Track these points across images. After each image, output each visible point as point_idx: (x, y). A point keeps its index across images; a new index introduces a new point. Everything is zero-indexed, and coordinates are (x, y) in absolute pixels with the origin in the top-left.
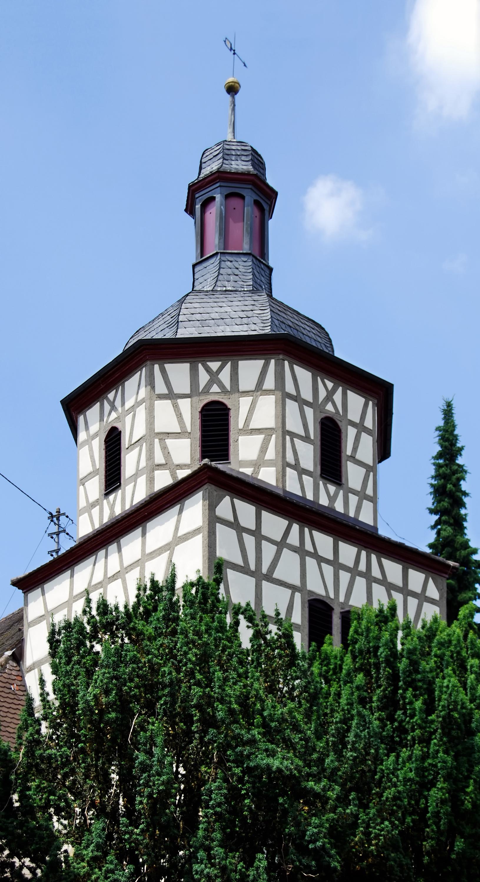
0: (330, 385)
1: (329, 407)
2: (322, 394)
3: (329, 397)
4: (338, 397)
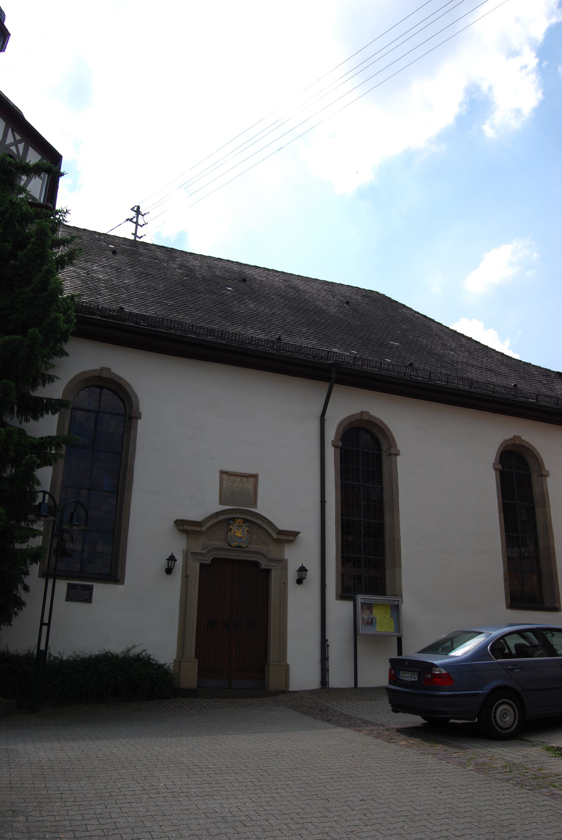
0: (18, 137)
1: (13, 148)
2: (10, 139)
3: (16, 143)
4: (21, 146)
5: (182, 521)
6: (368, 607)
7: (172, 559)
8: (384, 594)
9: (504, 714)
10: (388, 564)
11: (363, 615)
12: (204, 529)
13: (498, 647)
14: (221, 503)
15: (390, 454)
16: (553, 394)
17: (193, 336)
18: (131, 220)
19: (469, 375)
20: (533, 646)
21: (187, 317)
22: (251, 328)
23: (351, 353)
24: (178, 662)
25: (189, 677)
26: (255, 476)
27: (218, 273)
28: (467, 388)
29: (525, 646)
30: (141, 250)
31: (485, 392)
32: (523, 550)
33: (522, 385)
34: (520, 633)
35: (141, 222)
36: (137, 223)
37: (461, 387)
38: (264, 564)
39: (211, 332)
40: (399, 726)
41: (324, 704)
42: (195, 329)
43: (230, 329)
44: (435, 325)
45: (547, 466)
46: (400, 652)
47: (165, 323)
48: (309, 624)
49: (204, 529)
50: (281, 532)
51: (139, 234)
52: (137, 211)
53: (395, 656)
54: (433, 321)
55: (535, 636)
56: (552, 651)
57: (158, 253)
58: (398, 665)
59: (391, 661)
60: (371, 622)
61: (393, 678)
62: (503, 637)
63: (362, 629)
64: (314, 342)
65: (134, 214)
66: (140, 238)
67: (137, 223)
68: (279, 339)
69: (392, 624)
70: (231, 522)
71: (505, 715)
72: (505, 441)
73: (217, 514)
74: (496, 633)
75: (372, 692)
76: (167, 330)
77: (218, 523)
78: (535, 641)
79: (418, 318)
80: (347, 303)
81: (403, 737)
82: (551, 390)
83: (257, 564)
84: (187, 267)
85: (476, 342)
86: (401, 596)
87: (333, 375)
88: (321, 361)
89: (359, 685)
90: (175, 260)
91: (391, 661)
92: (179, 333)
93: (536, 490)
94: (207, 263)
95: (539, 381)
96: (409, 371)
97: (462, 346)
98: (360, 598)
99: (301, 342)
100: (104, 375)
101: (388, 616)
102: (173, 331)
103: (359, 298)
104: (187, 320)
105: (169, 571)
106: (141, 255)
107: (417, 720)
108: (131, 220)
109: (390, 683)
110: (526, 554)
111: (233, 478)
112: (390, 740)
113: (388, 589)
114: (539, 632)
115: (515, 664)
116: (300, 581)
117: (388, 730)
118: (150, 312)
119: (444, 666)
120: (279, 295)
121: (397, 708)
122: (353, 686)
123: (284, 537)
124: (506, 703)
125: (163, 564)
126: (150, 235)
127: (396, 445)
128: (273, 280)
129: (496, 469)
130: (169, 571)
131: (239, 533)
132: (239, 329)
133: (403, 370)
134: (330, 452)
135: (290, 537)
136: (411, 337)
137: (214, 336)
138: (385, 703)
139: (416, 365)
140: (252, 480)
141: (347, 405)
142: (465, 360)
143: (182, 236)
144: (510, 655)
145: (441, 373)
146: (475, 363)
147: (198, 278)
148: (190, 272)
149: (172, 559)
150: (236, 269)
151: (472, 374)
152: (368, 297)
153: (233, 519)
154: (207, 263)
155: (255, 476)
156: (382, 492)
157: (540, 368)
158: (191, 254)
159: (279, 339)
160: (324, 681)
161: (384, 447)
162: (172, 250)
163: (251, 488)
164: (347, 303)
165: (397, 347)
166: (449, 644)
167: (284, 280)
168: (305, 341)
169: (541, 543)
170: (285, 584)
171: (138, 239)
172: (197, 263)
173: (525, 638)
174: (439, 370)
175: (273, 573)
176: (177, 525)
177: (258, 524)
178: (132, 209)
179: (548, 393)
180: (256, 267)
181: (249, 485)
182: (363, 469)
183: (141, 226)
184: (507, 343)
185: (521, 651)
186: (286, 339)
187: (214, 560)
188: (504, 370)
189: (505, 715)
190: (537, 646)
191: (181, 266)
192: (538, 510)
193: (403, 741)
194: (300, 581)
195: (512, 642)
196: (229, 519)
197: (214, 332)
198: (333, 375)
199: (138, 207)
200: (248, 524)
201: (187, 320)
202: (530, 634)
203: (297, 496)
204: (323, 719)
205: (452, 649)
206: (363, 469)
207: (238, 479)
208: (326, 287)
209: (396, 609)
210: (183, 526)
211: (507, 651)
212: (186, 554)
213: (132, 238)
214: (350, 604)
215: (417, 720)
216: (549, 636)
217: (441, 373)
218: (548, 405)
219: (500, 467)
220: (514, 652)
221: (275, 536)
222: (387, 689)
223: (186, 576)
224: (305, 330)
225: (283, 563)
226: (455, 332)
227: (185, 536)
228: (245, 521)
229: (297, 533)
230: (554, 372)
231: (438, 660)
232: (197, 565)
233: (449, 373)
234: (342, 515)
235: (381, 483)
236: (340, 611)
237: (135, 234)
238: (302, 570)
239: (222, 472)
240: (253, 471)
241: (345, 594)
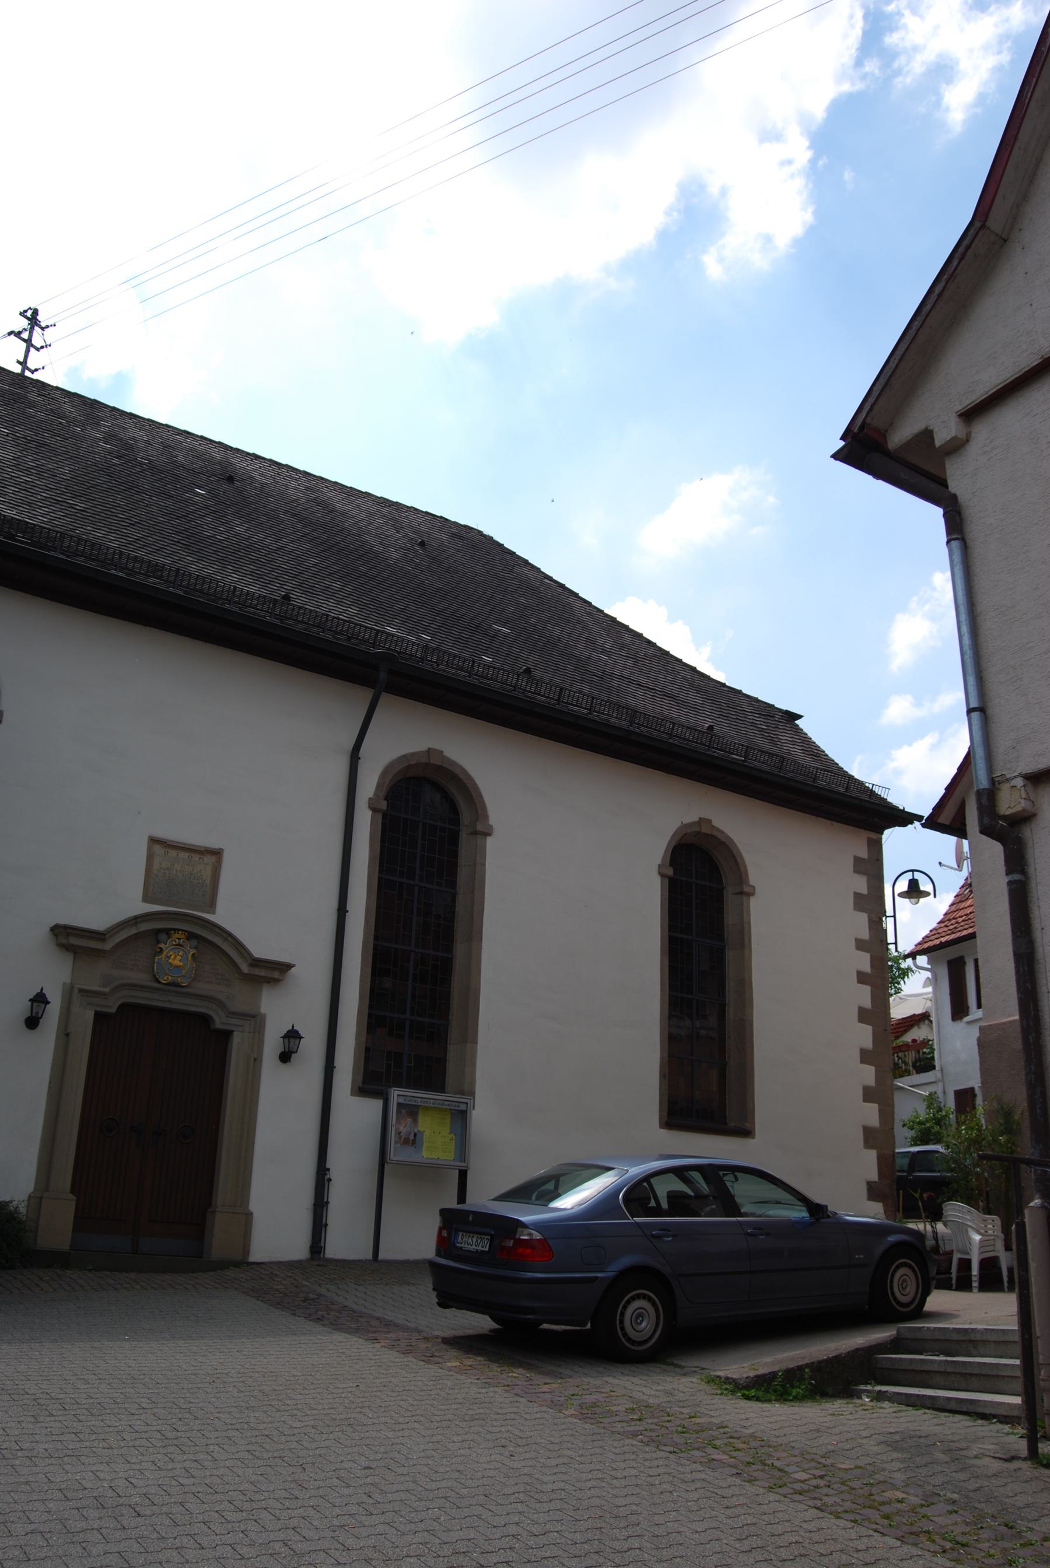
5: (66, 927)
6: (411, 1111)
7: (40, 999)
8: (441, 1089)
9: (639, 1316)
10: (453, 1034)
11: (398, 1126)
12: (108, 946)
13: (637, 1195)
14: (147, 898)
15: (475, 833)
16: (775, 750)
17: (120, 574)
18: (18, 334)
19: (632, 702)
20: (699, 1196)
21: (110, 536)
22: (235, 572)
23: (419, 638)
24: (37, 1199)
25: (57, 1229)
26: (217, 853)
27: (181, 459)
28: (624, 724)
29: (682, 1195)
30: (33, 396)
31: (655, 734)
32: (698, 1024)
33: (723, 729)
34: (679, 1172)
35: (37, 341)
36: (29, 342)
37: (613, 720)
38: (220, 1021)
39: (156, 569)
40: (448, 1333)
41: (314, 1289)
42: (124, 561)
43: (193, 568)
44: (579, 604)
45: (754, 876)
46: (462, 1198)
47: (67, 543)
48: (297, 1139)
49: (108, 946)
50: (257, 963)
51: (31, 364)
52: (33, 318)
53: (452, 1204)
54: (576, 595)
55: (705, 1178)
56: (731, 1207)
57: (67, 406)
58: (454, 1221)
59: (444, 1212)
60: (413, 1141)
61: (444, 1245)
62: (648, 1178)
63: (396, 1153)
64: (353, 611)
65: (24, 323)
66: (33, 372)
67: (29, 342)
68: (287, 598)
69: (452, 1147)
70: (163, 936)
71: (641, 1318)
72: (684, 826)
73: (136, 920)
74: (636, 1171)
75: (405, 1269)
76: (68, 556)
77: (136, 937)
78: (704, 1187)
79: (548, 587)
80: (422, 544)
81: (453, 1352)
82: (772, 741)
83: (205, 1020)
84: (121, 440)
85: (649, 642)
86: (472, 1094)
87: (383, 675)
88: (363, 647)
89: (382, 1256)
90: (98, 424)
91: (444, 1212)
92: (93, 565)
93: (730, 919)
94: (162, 438)
95: (753, 724)
96: (523, 683)
97: (623, 647)
98: (396, 1095)
99: (329, 607)
100: (433, 761)
101: (446, 1130)
102: (80, 560)
103: (444, 537)
104: (111, 541)
105: (32, 1022)
106: (32, 405)
107: (481, 1323)
108: (18, 334)
109: (438, 1253)
110: (703, 1032)
111: (173, 853)
112: (429, 1358)
113: (450, 1080)
114: (713, 1173)
115: (665, 1228)
116: (285, 1057)
117: (427, 1339)
118: (39, 518)
119: (539, 1226)
120: (294, 515)
121: (446, 1300)
122: (370, 1257)
123: (262, 973)
124: (645, 1297)
125: (22, 1008)
126: (54, 369)
127: (486, 817)
128: (286, 486)
129: (662, 875)
130: (32, 1022)
131: (176, 958)
132: (210, 571)
133: (512, 679)
134: (364, 821)
135: (274, 972)
136: (533, 620)
137: (160, 577)
138: (425, 1291)
139: (537, 674)
140: (209, 859)
141: (406, 733)
142: (626, 673)
143: (121, 380)
144: (658, 1212)
145: (580, 692)
146: (643, 680)
147: (141, 463)
148: (126, 450)
149: (40, 999)
150: (217, 455)
151: (638, 699)
152: (461, 537)
153: (167, 932)
154: (162, 438)
155: (217, 853)
156: (454, 900)
157: (756, 700)
158: (132, 416)
159: (287, 598)
160: (317, 1246)
161: (466, 817)
162: (95, 404)
163: (207, 874)
164: (422, 544)
165: (507, 635)
166: (550, 1186)
167: (307, 489)
168: (336, 607)
169: (731, 1013)
170: (257, 1060)
171: (27, 374)
172: (141, 435)
173: (686, 1181)
174: (578, 686)
175: (237, 1039)
176: (56, 935)
177: (213, 944)
178: (23, 314)
179: (767, 747)
180: (256, 457)
181: (203, 868)
182: (422, 848)
183: (38, 349)
184: (706, 651)
185: (679, 1204)
186: (299, 599)
187: (123, 1007)
188: (693, 697)
189: (641, 1318)
190: (707, 1196)
191: (109, 437)
192: (730, 955)
193: (453, 1360)
194: (285, 1057)
195: (663, 1188)
196: (159, 931)
197: (162, 571)
198: (383, 675)
199: (36, 312)
200: (194, 943)
201: (111, 541)
202: (696, 1176)
203: (294, 897)
204: (308, 1317)
205: (556, 1195)
206: (422, 848)
207: (184, 855)
208: (386, 510)
209: (461, 1118)
210: (67, 938)
211: (653, 1204)
212: (69, 993)
213: (17, 369)
214: (377, 1104)
215: (481, 1323)
216: (728, 1179)
217: (580, 692)
218: (764, 767)
219: (670, 872)
220: (665, 1205)
221: (245, 968)
222: (432, 1264)
223: (65, 1035)
224: (337, 585)
225: (256, 1020)
226: (614, 620)
227: (69, 958)
228: (191, 936)
229: (289, 966)
230: (780, 710)
231: (529, 1215)
232: (90, 1015)
233: (595, 693)
234: (376, 938)
235: (453, 884)
236: (357, 1117)
237: (23, 364)
238: (293, 1035)
239: (153, 841)
240: (213, 843)
241: (369, 1085)
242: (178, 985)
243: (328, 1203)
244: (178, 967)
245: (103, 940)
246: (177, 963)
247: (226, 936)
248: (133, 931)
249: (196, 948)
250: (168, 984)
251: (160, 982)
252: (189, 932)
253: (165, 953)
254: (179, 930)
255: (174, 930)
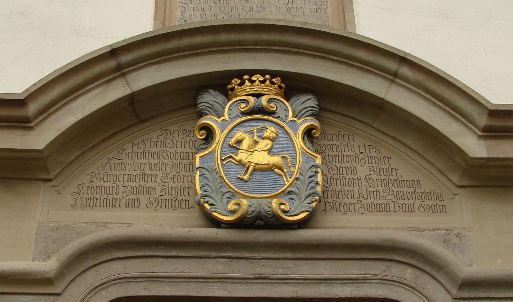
70: (210, 98)
153: (222, 83)
200: (309, 102)
242: (274, 222)
243: (31, 128)
244: (269, 169)
245: (24, 124)
246: (261, 158)
247: (392, 65)
248: (117, 91)
249: (315, 115)
250: (242, 223)
251: (217, 223)
252: (285, 76)
253: (219, 136)
254: (251, 73)
255: (239, 74)
